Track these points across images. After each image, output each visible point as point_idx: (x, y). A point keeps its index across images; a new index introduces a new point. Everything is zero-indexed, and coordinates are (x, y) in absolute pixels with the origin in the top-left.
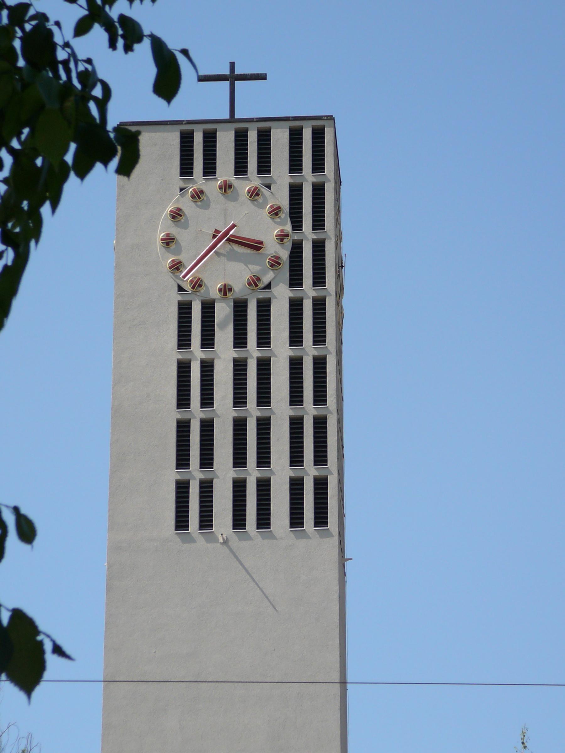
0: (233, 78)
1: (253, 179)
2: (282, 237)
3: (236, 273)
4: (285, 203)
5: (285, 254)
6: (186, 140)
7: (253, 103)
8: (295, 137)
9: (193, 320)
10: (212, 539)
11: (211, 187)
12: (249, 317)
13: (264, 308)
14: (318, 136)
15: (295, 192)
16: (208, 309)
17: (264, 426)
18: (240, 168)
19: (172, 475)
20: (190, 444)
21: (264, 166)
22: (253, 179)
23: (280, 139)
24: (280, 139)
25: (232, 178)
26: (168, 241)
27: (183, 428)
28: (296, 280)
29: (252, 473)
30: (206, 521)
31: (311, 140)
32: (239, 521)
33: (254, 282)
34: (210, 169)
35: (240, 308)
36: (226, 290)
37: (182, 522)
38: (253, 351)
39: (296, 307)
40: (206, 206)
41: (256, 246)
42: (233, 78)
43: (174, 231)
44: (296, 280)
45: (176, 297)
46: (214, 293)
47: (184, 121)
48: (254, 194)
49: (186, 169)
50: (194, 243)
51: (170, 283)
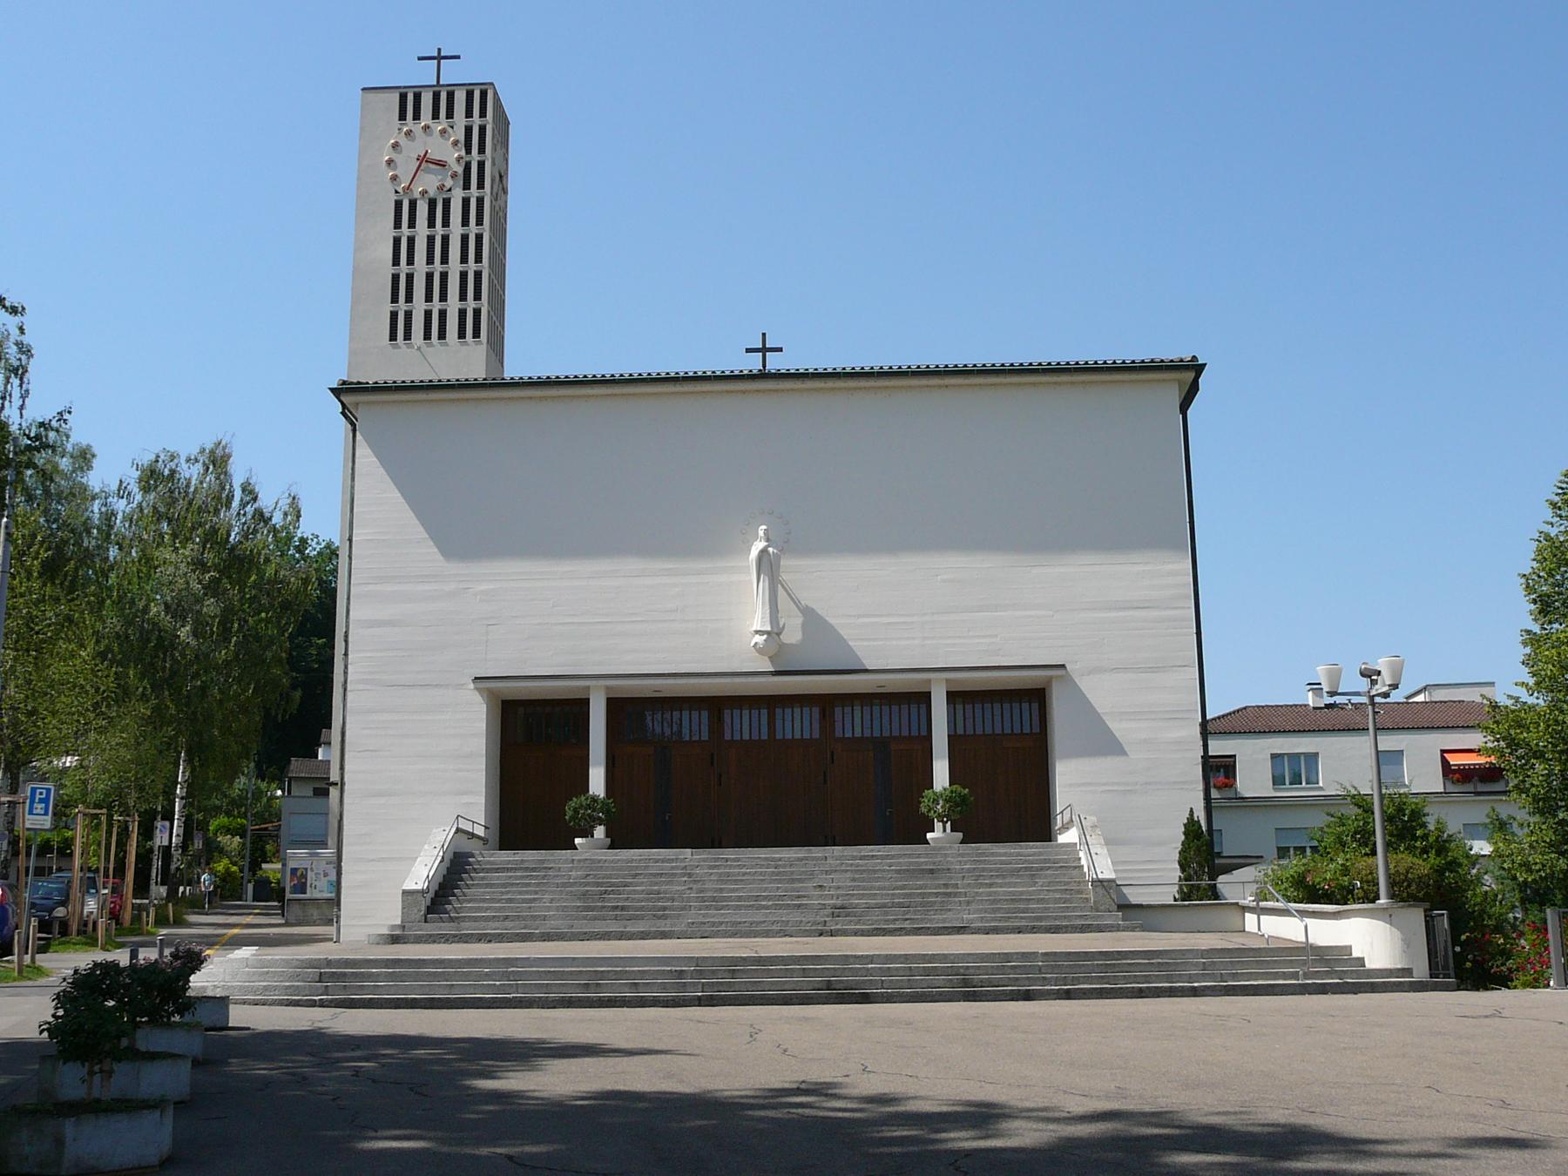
0: (439, 58)
1: (443, 123)
2: (459, 159)
3: (429, 183)
4: (462, 139)
5: (460, 170)
6: (403, 98)
7: (452, 74)
8: (470, 95)
9: (404, 212)
10: (410, 346)
11: (417, 128)
12: (438, 208)
13: (447, 203)
14: (484, 94)
15: (469, 130)
16: (413, 204)
17: (444, 276)
18: (436, 116)
19: (391, 233)
20: (400, 288)
21: (450, 115)
22: (443, 123)
23: (460, 97)
24: (460, 97)
25: (430, 122)
26: (390, 162)
27: (395, 278)
28: (467, 186)
29: (436, 306)
30: (408, 336)
31: (481, 97)
32: (427, 336)
33: (441, 188)
34: (417, 117)
35: (432, 204)
36: (424, 192)
37: (393, 337)
38: (439, 230)
39: (466, 202)
40: (413, 140)
41: (441, 164)
42: (439, 58)
43: (394, 156)
44: (467, 186)
45: (394, 197)
46: (417, 195)
47: (1526, 985)
48: (443, 132)
49: (402, 117)
50: (406, 169)
51: (390, 188)
